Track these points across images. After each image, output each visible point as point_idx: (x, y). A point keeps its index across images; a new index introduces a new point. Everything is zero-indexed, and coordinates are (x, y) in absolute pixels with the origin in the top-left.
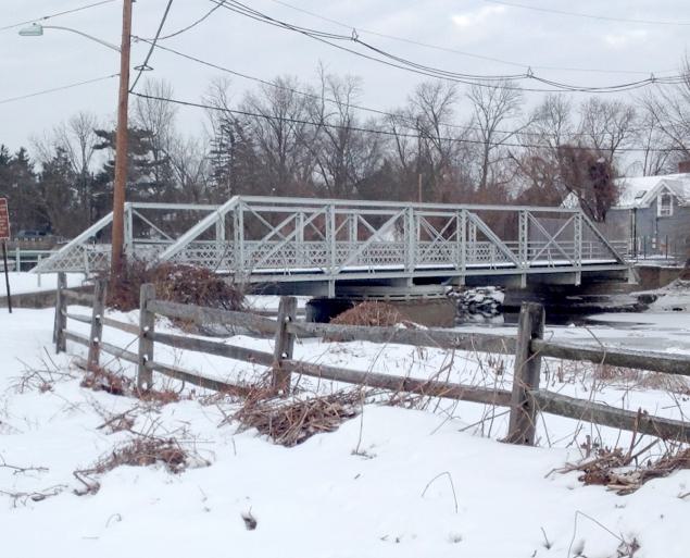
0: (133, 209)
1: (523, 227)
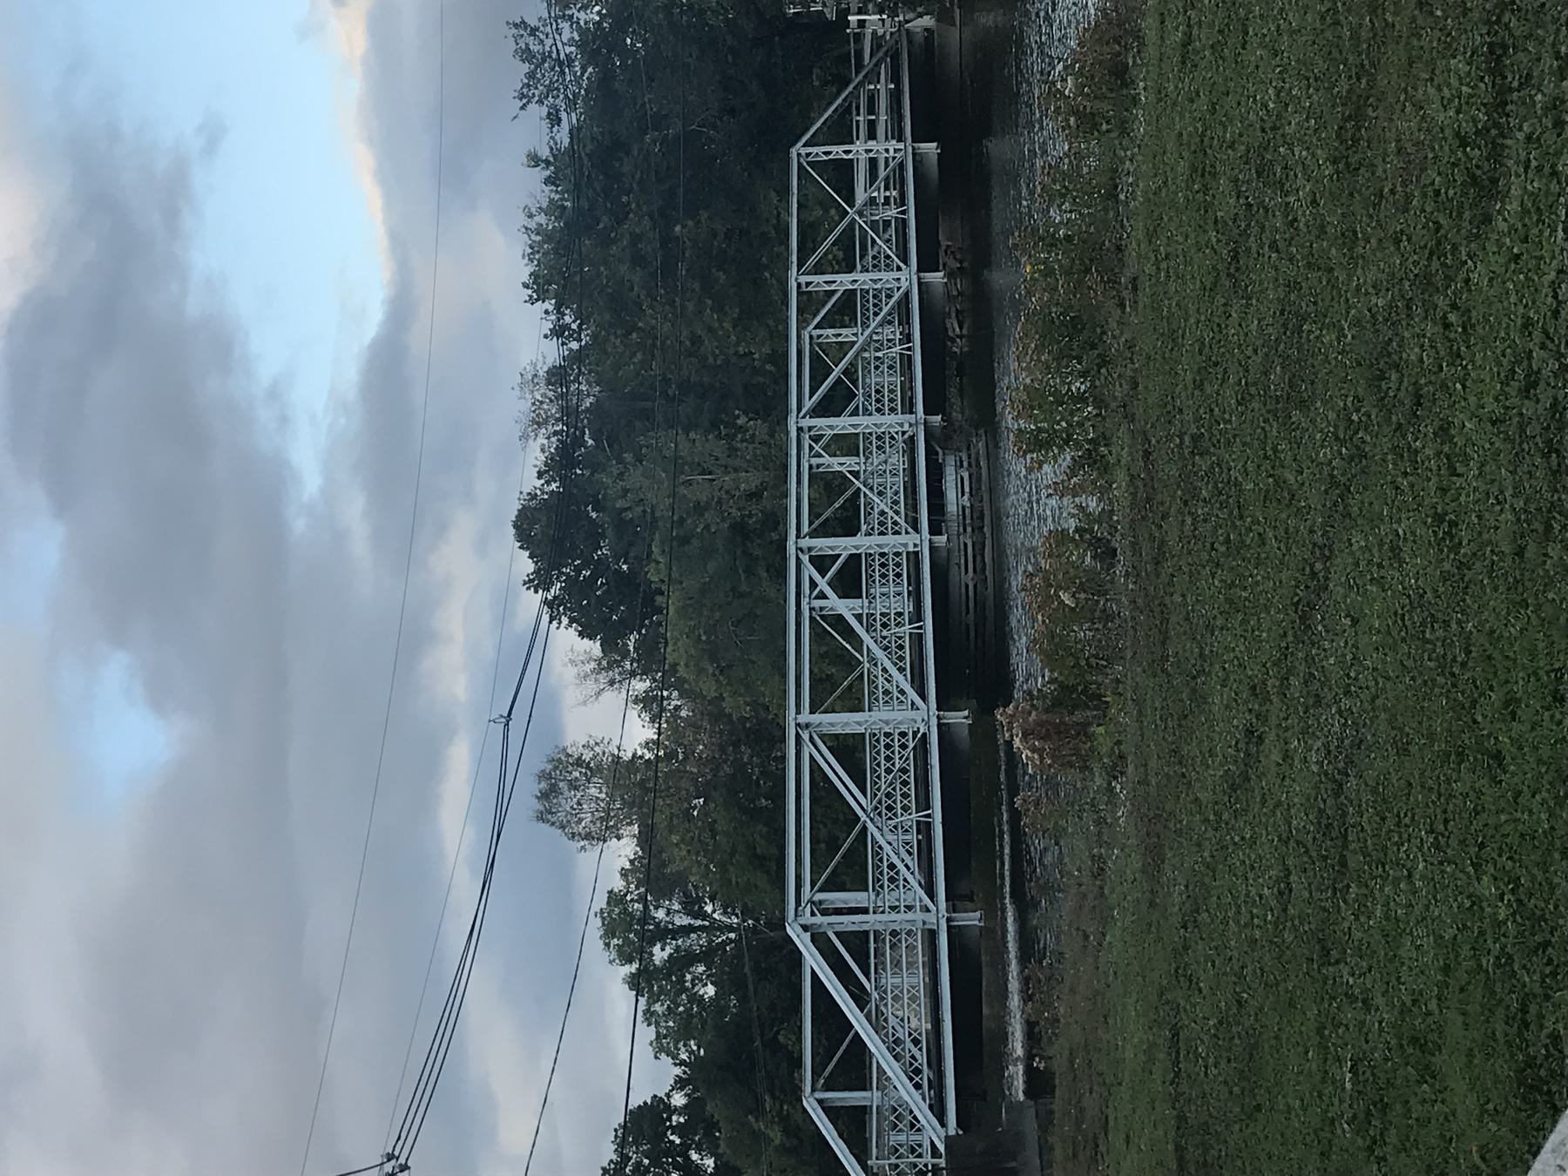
0: (813, 1090)
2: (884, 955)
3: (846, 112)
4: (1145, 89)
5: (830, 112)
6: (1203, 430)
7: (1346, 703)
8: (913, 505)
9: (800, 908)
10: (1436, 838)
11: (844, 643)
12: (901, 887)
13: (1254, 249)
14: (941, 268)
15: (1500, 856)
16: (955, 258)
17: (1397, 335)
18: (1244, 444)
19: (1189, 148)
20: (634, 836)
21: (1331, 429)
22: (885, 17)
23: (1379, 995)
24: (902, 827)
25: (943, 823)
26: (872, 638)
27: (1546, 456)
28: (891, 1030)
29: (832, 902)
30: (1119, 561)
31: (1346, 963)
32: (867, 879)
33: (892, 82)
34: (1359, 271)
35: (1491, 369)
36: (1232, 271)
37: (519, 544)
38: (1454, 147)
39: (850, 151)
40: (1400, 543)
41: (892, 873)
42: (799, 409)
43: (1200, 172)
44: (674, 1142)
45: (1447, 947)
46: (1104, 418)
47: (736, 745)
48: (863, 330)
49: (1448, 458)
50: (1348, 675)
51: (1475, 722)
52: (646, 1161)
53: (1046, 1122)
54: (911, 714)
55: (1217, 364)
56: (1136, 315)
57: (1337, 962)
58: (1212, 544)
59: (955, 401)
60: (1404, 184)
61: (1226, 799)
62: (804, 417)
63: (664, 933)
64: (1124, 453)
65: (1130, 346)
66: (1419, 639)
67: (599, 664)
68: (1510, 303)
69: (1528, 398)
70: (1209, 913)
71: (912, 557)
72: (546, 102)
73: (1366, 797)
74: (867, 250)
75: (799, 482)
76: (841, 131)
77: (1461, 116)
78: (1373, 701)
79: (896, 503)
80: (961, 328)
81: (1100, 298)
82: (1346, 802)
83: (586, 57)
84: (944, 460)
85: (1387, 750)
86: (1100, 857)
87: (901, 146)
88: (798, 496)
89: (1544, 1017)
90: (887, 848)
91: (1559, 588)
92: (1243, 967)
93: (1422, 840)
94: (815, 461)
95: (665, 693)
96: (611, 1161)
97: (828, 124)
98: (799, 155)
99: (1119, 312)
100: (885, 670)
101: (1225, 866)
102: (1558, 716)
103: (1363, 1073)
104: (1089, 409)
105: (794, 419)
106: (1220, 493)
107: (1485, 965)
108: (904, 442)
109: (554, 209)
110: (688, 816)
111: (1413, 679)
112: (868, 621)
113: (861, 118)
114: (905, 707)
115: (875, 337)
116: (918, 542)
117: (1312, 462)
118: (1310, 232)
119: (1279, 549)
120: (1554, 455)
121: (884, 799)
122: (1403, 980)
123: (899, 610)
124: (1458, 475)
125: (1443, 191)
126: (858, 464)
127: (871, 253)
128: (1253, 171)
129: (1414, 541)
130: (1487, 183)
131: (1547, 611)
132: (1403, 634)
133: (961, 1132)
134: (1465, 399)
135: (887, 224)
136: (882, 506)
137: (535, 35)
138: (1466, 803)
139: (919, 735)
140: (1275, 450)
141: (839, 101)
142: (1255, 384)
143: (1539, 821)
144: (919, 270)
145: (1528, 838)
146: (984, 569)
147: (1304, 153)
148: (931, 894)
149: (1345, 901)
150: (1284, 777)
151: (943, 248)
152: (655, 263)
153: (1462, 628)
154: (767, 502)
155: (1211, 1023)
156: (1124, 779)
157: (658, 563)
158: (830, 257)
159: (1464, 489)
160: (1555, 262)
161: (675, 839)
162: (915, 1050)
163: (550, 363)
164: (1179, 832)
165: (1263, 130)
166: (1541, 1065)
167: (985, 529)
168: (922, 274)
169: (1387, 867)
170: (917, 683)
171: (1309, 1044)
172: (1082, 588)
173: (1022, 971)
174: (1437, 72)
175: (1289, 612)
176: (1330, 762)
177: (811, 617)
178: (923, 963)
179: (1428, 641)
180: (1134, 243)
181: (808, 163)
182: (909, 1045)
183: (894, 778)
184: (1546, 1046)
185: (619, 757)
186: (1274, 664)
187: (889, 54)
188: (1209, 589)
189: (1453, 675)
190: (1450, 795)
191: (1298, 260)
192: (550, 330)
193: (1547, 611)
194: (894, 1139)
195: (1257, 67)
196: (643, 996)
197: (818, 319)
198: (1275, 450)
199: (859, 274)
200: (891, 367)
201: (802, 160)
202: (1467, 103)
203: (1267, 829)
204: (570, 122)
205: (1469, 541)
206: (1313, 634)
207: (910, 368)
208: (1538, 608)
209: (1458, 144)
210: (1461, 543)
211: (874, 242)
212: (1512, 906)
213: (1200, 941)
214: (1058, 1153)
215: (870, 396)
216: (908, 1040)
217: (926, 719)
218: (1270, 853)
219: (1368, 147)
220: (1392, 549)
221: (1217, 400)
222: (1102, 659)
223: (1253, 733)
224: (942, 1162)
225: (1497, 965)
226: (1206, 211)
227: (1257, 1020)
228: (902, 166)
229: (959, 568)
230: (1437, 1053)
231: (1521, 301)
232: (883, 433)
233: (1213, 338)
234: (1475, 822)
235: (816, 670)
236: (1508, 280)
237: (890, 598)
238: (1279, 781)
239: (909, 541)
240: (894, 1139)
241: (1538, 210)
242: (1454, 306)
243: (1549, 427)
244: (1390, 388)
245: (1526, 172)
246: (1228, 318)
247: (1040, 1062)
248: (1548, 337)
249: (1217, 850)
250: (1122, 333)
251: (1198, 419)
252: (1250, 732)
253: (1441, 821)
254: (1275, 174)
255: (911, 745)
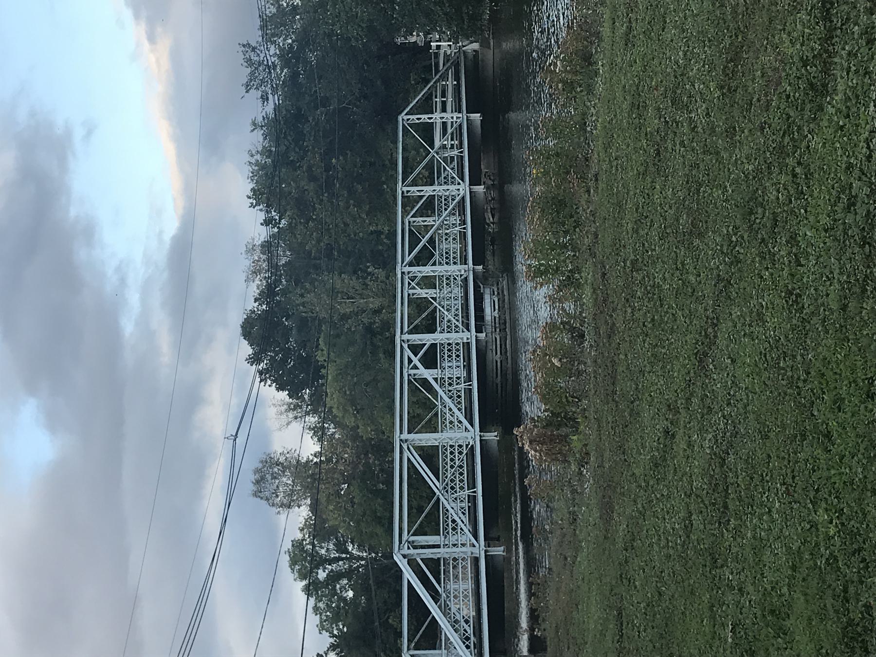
0: (409, 649)
3: (429, 98)
5: (420, 96)
6: (638, 257)
8: (466, 316)
9: (402, 545)
11: (427, 394)
12: (459, 533)
13: (670, 146)
14: (482, 183)
15: (830, 496)
19: (630, 93)
21: (719, 248)
22: (451, 43)
23: (750, 585)
24: (460, 499)
26: (443, 391)
27: (862, 247)
28: (453, 615)
30: (586, 340)
31: (727, 566)
33: (455, 81)
35: (825, 197)
38: (799, 67)
39: (432, 118)
40: (764, 311)
41: (453, 525)
42: (402, 262)
43: (636, 107)
45: (794, 554)
46: (578, 257)
47: (366, 454)
48: (439, 219)
50: (729, 394)
51: (813, 415)
54: (465, 434)
56: (597, 195)
57: (722, 566)
60: (766, 95)
61: (652, 472)
62: (405, 266)
63: (325, 561)
64: (589, 276)
65: (593, 214)
66: (775, 368)
67: (289, 407)
68: (838, 156)
72: (260, 89)
75: (402, 304)
76: (426, 106)
77: (804, 47)
78: (745, 407)
81: (576, 188)
82: (727, 470)
83: (283, 63)
84: (484, 290)
85: (754, 436)
87: (460, 115)
88: (402, 311)
89: (859, 595)
92: (662, 572)
93: (777, 489)
94: (411, 292)
97: (419, 102)
98: (403, 120)
99: (587, 195)
100: (450, 410)
101: (651, 512)
102: (870, 406)
105: (400, 267)
106: (649, 293)
108: (461, 281)
109: (266, 152)
110: (338, 493)
111: (771, 392)
112: (441, 382)
113: (438, 100)
114: (461, 431)
115: (445, 222)
116: (469, 337)
117: (706, 268)
118: (704, 133)
119: (685, 322)
120: (867, 246)
121: (449, 482)
123: (459, 376)
124: (802, 266)
125: (792, 94)
126: (436, 293)
127: (443, 176)
128: (669, 101)
130: (820, 87)
131: (864, 341)
135: (452, 158)
136: (449, 316)
137: (255, 51)
139: (469, 446)
140: (683, 264)
143: (856, 473)
144: (470, 185)
145: (848, 484)
146: (506, 352)
147: (702, 86)
148: (476, 537)
152: (321, 179)
153: (804, 359)
155: (642, 605)
156: (588, 467)
157: (322, 350)
159: (806, 273)
161: (331, 507)
162: (466, 627)
163: (262, 239)
164: (623, 494)
165: (676, 77)
166: (858, 624)
167: (507, 330)
168: (472, 187)
169: (755, 508)
170: (468, 417)
171: (704, 616)
172: (564, 356)
173: (528, 580)
174: (787, 24)
175: (692, 359)
176: (717, 446)
178: (471, 577)
179: (783, 369)
180: (596, 154)
181: (408, 124)
182: (463, 623)
184: (862, 613)
186: (682, 391)
187: (454, 64)
188: (642, 349)
189: (798, 387)
192: (264, 220)
193: (864, 341)
195: (672, 41)
197: (414, 211)
198: (683, 264)
199: (436, 186)
200: (454, 239)
201: (404, 122)
202: (808, 39)
203: (677, 489)
204: (274, 101)
205: (809, 305)
206: (707, 370)
207: (465, 239)
208: (857, 340)
209: (801, 65)
210: (803, 307)
211: (445, 169)
213: (635, 558)
215: (442, 255)
216: (462, 620)
217: (473, 437)
218: (679, 503)
219: (743, 76)
220: (758, 314)
221: (647, 238)
223: (668, 432)
227: (670, 603)
228: (460, 126)
229: (492, 352)
230: (787, 619)
231: (845, 154)
232: (450, 276)
233: (644, 202)
235: (411, 412)
237: (453, 369)
238: (685, 460)
239: (463, 336)
241: (858, 97)
242: (799, 163)
245: (848, 74)
246: (654, 189)
247: (538, 632)
249: (646, 503)
251: (635, 250)
252: (667, 432)
253: (791, 477)
254: (683, 102)
255: (465, 452)
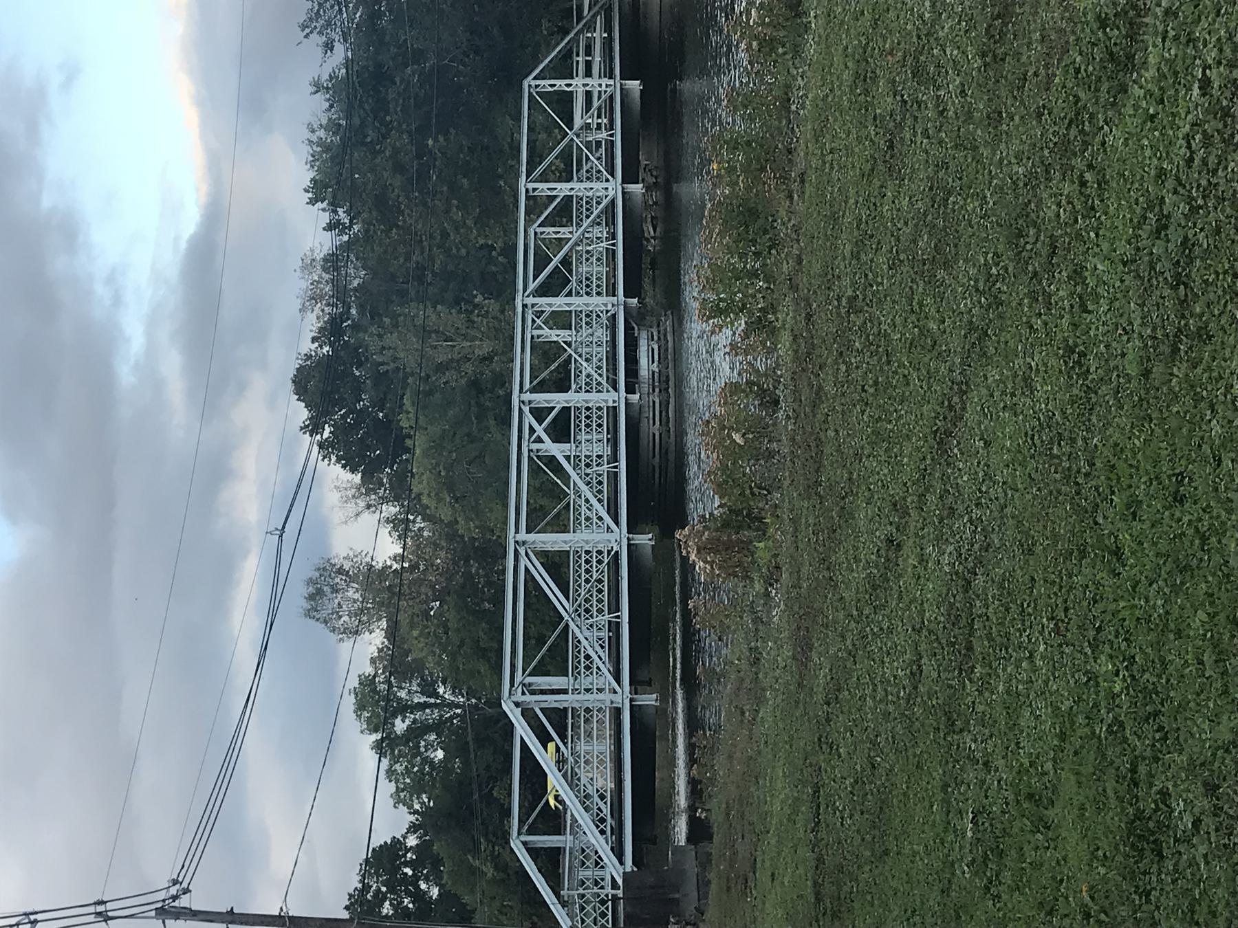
0: (519, 834)
1: (552, 86)
2: (579, 727)
3: (567, 55)
4: (815, 17)
7: (976, 513)
8: (613, 368)
10: (1056, 625)
15: (1117, 637)
16: (652, 175)
17: (1036, 196)
18: (894, 302)
20: (382, 629)
25: (629, 623)
27: (1175, 288)
28: (583, 787)
29: (539, 685)
31: (969, 731)
32: (568, 667)
34: (1003, 146)
35: (1124, 216)
36: (887, 158)
37: (297, 397)
39: (571, 85)
42: (524, 291)
44: (406, 874)
47: (467, 561)
49: (1080, 298)
51: (1096, 523)
52: (384, 889)
53: (705, 862)
54: (607, 536)
55: (872, 236)
57: (962, 731)
58: (863, 386)
59: (650, 293)
60: (1047, 67)
61: (867, 597)
62: (528, 296)
63: (403, 709)
66: (1046, 455)
69: (1158, 238)
70: (850, 692)
71: (611, 409)
73: (993, 591)
74: (582, 165)
76: (563, 68)
79: (599, 368)
80: (655, 232)
81: (773, 191)
86: (757, 648)
87: (611, 82)
88: (522, 360)
90: (584, 642)
91: (1184, 402)
93: (1043, 626)
94: (536, 333)
95: (411, 517)
96: (356, 888)
98: (530, 86)
100: (587, 501)
102: (1178, 514)
103: (983, 824)
104: (761, 284)
105: (520, 297)
106: (871, 344)
107: (1098, 732)
109: (333, 127)
110: (426, 614)
111: (1039, 489)
112: (575, 461)
113: (580, 59)
115: (587, 235)
117: (954, 312)
119: (922, 388)
120: (1182, 287)
121: (583, 603)
122: (1022, 745)
123: (600, 453)
124: (1089, 312)
128: (909, 72)
129: (1046, 372)
130: (1123, 59)
132: (1032, 451)
133: (635, 869)
134: (1098, 246)
135: (598, 144)
136: (589, 369)
138: (1085, 593)
140: (921, 304)
141: (563, 44)
142: (904, 251)
144: (624, 182)
145: (1143, 621)
146: (668, 422)
148: (618, 679)
149: (970, 680)
150: (919, 577)
151: (643, 167)
154: (496, 366)
155: (847, 782)
157: (408, 413)
158: (553, 168)
159: (1093, 323)
160: (1190, 117)
161: (415, 633)
163: (325, 251)
165: (919, 37)
166: (1150, 818)
170: (612, 511)
176: (960, 563)
177: (529, 456)
181: (537, 93)
182: (597, 799)
183: (592, 587)
184: (1155, 802)
185: (372, 566)
189: (1077, 484)
190: (1071, 587)
191: (946, 143)
194: (584, 874)
196: (386, 757)
197: (542, 218)
198: (921, 304)
205: (1097, 368)
206: (949, 456)
207: (614, 260)
211: (588, 159)
212: (1126, 681)
213: (840, 715)
214: (714, 887)
215: (581, 282)
216: (596, 795)
220: (1025, 380)
221: (871, 267)
222: (765, 489)
223: (892, 541)
224: (620, 893)
225: (1110, 731)
226: (867, 110)
228: (611, 97)
232: (591, 312)
233: (869, 215)
234: (1093, 609)
235: (532, 501)
236: (1143, 137)
237: (592, 444)
239: (608, 398)
240: (584, 874)
243: (1178, 262)
244: (1027, 243)
248: (1180, 184)
250: (790, 220)
251: (854, 283)
252: (890, 541)
254: (928, 74)
255: (606, 561)
